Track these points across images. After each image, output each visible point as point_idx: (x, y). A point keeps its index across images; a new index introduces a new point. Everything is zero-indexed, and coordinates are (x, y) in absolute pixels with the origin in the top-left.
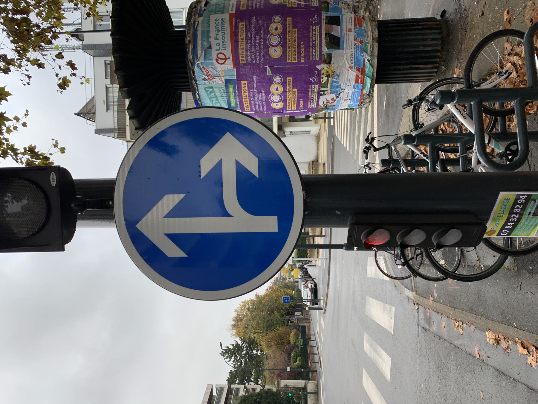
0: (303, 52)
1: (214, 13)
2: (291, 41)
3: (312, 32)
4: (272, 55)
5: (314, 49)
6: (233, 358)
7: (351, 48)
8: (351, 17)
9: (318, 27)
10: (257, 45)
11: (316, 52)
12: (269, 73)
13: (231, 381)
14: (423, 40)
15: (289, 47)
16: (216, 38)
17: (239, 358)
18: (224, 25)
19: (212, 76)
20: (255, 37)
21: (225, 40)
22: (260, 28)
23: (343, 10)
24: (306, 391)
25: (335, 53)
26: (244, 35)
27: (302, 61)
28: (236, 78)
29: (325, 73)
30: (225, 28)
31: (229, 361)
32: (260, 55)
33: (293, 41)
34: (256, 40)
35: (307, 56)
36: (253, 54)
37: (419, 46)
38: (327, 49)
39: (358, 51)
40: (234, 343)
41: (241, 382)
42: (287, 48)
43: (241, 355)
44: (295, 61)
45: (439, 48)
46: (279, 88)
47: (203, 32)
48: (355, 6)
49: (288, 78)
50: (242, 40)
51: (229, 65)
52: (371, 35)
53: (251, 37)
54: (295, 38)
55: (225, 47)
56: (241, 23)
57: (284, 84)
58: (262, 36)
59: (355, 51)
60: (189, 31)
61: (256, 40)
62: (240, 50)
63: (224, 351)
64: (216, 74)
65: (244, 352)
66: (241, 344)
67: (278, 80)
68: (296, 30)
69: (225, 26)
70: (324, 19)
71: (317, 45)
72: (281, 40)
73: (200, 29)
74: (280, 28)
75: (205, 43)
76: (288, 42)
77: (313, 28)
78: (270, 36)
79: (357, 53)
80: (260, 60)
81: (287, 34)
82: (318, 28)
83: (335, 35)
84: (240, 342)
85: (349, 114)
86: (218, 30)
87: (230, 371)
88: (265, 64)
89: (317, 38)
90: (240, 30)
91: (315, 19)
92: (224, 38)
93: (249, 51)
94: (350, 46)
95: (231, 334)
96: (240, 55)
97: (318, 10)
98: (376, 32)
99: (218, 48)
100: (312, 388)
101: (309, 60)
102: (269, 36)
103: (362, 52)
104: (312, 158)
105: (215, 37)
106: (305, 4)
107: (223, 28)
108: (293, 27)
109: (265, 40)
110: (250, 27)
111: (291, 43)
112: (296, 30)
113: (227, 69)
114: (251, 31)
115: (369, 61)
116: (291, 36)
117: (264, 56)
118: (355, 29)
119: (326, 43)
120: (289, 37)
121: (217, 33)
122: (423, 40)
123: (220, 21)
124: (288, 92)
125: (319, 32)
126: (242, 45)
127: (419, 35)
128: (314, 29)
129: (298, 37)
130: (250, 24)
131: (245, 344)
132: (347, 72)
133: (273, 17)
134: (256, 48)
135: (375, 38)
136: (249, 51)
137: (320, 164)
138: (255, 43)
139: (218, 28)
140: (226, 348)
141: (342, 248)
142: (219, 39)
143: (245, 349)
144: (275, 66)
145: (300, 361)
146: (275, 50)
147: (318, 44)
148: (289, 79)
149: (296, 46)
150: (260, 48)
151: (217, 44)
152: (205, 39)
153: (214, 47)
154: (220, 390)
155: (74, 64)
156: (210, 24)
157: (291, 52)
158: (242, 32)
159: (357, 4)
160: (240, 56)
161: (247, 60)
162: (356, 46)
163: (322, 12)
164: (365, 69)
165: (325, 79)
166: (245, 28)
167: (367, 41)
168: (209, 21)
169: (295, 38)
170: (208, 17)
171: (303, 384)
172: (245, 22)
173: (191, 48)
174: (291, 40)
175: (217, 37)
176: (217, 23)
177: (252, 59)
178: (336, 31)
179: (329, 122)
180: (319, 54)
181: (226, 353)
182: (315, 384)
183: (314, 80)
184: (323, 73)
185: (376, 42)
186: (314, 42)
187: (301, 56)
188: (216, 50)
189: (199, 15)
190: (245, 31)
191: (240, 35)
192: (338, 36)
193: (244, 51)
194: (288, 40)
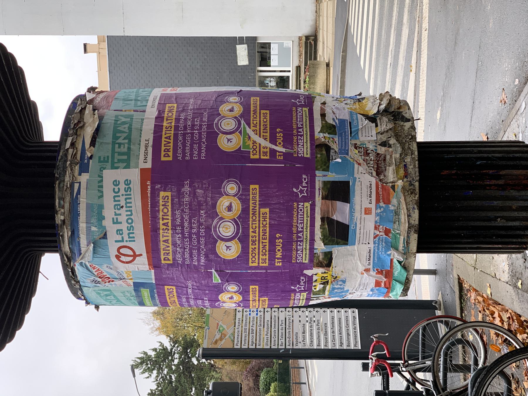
0: (279, 250)
1: (109, 165)
2: (257, 231)
3: (297, 215)
4: (221, 254)
5: (300, 245)
6: (155, 372)
7: (367, 242)
8: (371, 185)
9: (307, 205)
10: (194, 236)
11: (304, 250)
12: (216, 279)
14: (502, 209)
15: (254, 242)
16: (115, 221)
18: (130, 195)
19: (109, 278)
20: (190, 223)
21: (133, 224)
22: (200, 204)
23: (356, 166)
25: (337, 251)
26: (170, 218)
27: (278, 264)
28: (154, 282)
30: (133, 202)
31: (148, 377)
33: (261, 231)
34: (191, 228)
35: (287, 257)
36: (187, 250)
38: (324, 245)
39: (380, 246)
40: (157, 346)
42: (250, 244)
43: (169, 367)
44: (264, 265)
46: (233, 204)
47: (89, 207)
48: (378, 154)
49: (252, 187)
50: (165, 227)
52: (405, 220)
54: (264, 226)
55: (134, 237)
56: (162, 194)
57: (244, 200)
58: (202, 221)
59: (374, 247)
60: (62, 202)
61: (191, 228)
62: (162, 243)
63: (139, 361)
64: (116, 275)
65: (176, 362)
67: (232, 188)
68: (267, 210)
69: (133, 198)
70: (319, 189)
71: (306, 239)
72: (238, 229)
73: (83, 201)
75: (93, 229)
76: (251, 234)
77: (298, 208)
78: (218, 223)
79: (378, 249)
81: (251, 219)
82: (309, 208)
83: (340, 220)
84: (168, 345)
86: (120, 205)
87: (150, 392)
88: (207, 267)
89: (307, 227)
90: (161, 207)
91: (301, 190)
93: (179, 245)
94: (368, 239)
95: (151, 328)
96: (162, 251)
98: (416, 215)
99: (119, 238)
101: (292, 263)
103: (387, 249)
105: (113, 219)
106: (284, 150)
107: (128, 201)
108: (262, 206)
109: (208, 229)
110: (179, 201)
111: (257, 235)
112: (267, 210)
113: (137, 270)
114: (182, 210)
115: (400, 262)
116: (257, 222)
117: (206, 256)
118: (376, 209)
120: (253, 225)
121: (118, 212)
122: (502, 209)
123: (122, 186)
124: (251, 302)
125: (309, 215)
127: (496, 200)
128: (301, 210)
129: (269, 224)
130: (179, 195)
131: (178, 347)
132: (359, 276)
133: (224, 184)
134: (191, 240)
135: (413, 226)
136: (179, 245)
138: (190, 234)
139: (119, 201)
140: (142, 355)
142: (121, 223)
143: (176, 356)
144: (227, 271)
146: (228, 247)
147: (307, 236)
148: (254, 188)
151: (117, 231)
152: (93, 220)
153: (113, 236)
156: (102, 192)
157: (257, 250)
158: (165, 210)
159: (383, 149)
160: (162, 252)
161: (174, 259)
162: (377, 239)
164: (392, 272)
165: (319, 287)
167: (397, 232)
168: (100, 184)
169: (264, 226)
172: (171, 191)
173: (66, 233)
174: (257, 229)
175: (117, 219)
176: (116, 190)
177: (184, 259)
180: (310, 254)
181: (142, 363)
184: (316, 280)
186: (300, 130)
187: (277, 257)
188: (116, 241)
189: (80, 167)
190: (170, 209)
191: (161, 216)
192: (345, 222)
193: (170, 245)
194: (251, 230)
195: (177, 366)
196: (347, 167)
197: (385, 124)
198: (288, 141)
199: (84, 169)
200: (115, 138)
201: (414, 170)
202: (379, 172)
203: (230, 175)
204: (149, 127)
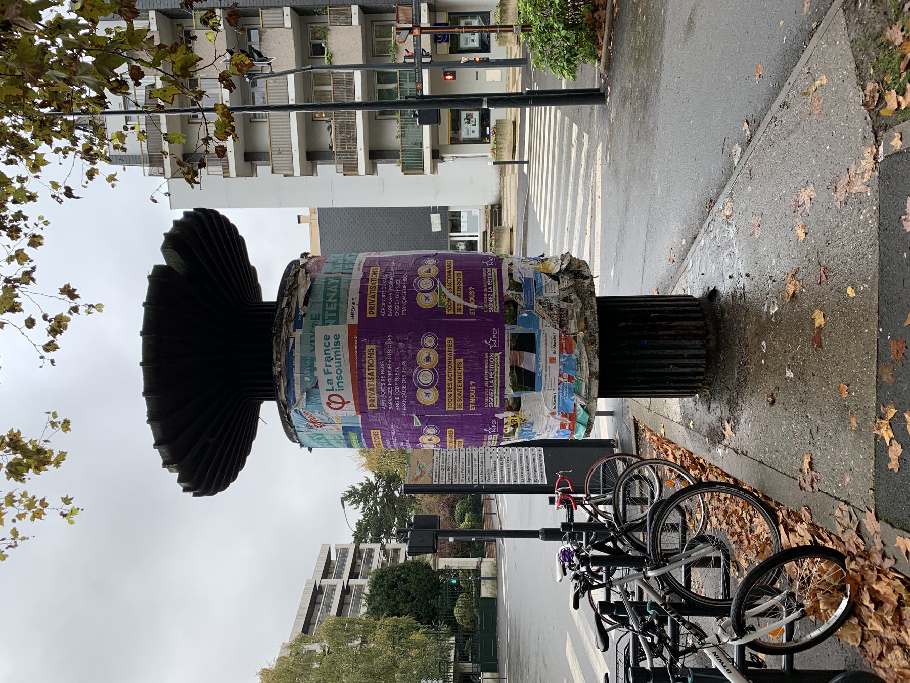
6: (362, 504)
9: (498, 355)
10: (397, 385)
12: (417, 423)
13: (359, 537)
14: (675, 357)
15: (450, 388)
17: (371, 504)
20: (393, 372)
23: (541, 319)
24: (479, 575)
25: (525, 396)
29: (509, 423)
32: (401, 400)
35: (480, 403)
36: (390, 397)
37: (668, 366)
40: (364, 481)
41: (376, 540)
43: (374, 499)
44: (459, 313)
45: (702, 370)
47: (303, 359)
48: (561, 309)
51: (350, 410)
53: (386, 372)
54: (459, 374)
56: (368, 347)
58: (404, 370)
60: (279, 356)
61: (394, 377)
62: (368, 391)
65: (380, 494)
66: (374, 482)
67: (430, 341)
68: (462, 360)
71: (496, 292)
72: (436, 378)
74: (435, 357)
75: (307, 379)
76: (447, 382)
78: (418, 372)
79: (563, 395)
80: (401, 406)
83: (527, 368)
84: (373, 479)
85: (556, 148)
90: (367, 359)
92: (339, 371)
97: (499, 321)
98: (596, 363)
99: (329, 387)
100: (488, 570)
102: (415, 371)
104: (491, 200)
106: (476, 306)
108: (457, 357)
109: (409, 377)
111: (453, 382)
112: (462, 360)
115: (583, 406)
117: (408, 402)
119: (512, 382)
120: (449, 374)
121: (328, 364)
122: (675, 357)
123: (332, 341)
126: (371, 384)
130: (383, 347)
132: (546, 419)
134: (393, 388)
135: (594, 373)
137: (504, 229)
138: (393, 382)
140: (351, 489)
141: (538, 537)
142: (331, 373)
143: (381, 489)
145: (469, 521)
146: (427, 394)
148: (450, 341)
149: (462, 388)
150: (401, 390)
153: (323, 386)
154: (343, 553)
155: (74, 290)
156: (314, 346)
157: (453, 396)
158: (371, 362)
159: (565, 304)
160: (368, 399)
161: (379, 406)
162: (561, 385)
163: (505, 325)
166: (374, 356)
169: (459, 374)
170: (312, 332)
171: (475, 565)
172: (376, 344)
173: (283, 384)
174: (453, 378)
177: (388, 405)
178: (528, 362)
179: (521, 170)
180: (500, 399)
181: (350, 496)
182: (493, 563)
183: (492, 343)
185: (596, 379)
186: (490, 288)
188: (327, 390)
189: (295, 324)
191: (367, 367)
194: (447, 378)
195: (381, 498)
196: (532, 320)
197: (566, 282)
198: (479, 298)
199: (299, 325)
200: (325, 297)
201: (593, 322)
202: (562, 324)
203: (428, 329)
204: (355, 287)
